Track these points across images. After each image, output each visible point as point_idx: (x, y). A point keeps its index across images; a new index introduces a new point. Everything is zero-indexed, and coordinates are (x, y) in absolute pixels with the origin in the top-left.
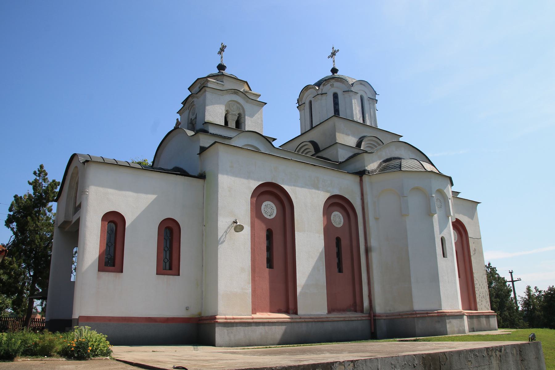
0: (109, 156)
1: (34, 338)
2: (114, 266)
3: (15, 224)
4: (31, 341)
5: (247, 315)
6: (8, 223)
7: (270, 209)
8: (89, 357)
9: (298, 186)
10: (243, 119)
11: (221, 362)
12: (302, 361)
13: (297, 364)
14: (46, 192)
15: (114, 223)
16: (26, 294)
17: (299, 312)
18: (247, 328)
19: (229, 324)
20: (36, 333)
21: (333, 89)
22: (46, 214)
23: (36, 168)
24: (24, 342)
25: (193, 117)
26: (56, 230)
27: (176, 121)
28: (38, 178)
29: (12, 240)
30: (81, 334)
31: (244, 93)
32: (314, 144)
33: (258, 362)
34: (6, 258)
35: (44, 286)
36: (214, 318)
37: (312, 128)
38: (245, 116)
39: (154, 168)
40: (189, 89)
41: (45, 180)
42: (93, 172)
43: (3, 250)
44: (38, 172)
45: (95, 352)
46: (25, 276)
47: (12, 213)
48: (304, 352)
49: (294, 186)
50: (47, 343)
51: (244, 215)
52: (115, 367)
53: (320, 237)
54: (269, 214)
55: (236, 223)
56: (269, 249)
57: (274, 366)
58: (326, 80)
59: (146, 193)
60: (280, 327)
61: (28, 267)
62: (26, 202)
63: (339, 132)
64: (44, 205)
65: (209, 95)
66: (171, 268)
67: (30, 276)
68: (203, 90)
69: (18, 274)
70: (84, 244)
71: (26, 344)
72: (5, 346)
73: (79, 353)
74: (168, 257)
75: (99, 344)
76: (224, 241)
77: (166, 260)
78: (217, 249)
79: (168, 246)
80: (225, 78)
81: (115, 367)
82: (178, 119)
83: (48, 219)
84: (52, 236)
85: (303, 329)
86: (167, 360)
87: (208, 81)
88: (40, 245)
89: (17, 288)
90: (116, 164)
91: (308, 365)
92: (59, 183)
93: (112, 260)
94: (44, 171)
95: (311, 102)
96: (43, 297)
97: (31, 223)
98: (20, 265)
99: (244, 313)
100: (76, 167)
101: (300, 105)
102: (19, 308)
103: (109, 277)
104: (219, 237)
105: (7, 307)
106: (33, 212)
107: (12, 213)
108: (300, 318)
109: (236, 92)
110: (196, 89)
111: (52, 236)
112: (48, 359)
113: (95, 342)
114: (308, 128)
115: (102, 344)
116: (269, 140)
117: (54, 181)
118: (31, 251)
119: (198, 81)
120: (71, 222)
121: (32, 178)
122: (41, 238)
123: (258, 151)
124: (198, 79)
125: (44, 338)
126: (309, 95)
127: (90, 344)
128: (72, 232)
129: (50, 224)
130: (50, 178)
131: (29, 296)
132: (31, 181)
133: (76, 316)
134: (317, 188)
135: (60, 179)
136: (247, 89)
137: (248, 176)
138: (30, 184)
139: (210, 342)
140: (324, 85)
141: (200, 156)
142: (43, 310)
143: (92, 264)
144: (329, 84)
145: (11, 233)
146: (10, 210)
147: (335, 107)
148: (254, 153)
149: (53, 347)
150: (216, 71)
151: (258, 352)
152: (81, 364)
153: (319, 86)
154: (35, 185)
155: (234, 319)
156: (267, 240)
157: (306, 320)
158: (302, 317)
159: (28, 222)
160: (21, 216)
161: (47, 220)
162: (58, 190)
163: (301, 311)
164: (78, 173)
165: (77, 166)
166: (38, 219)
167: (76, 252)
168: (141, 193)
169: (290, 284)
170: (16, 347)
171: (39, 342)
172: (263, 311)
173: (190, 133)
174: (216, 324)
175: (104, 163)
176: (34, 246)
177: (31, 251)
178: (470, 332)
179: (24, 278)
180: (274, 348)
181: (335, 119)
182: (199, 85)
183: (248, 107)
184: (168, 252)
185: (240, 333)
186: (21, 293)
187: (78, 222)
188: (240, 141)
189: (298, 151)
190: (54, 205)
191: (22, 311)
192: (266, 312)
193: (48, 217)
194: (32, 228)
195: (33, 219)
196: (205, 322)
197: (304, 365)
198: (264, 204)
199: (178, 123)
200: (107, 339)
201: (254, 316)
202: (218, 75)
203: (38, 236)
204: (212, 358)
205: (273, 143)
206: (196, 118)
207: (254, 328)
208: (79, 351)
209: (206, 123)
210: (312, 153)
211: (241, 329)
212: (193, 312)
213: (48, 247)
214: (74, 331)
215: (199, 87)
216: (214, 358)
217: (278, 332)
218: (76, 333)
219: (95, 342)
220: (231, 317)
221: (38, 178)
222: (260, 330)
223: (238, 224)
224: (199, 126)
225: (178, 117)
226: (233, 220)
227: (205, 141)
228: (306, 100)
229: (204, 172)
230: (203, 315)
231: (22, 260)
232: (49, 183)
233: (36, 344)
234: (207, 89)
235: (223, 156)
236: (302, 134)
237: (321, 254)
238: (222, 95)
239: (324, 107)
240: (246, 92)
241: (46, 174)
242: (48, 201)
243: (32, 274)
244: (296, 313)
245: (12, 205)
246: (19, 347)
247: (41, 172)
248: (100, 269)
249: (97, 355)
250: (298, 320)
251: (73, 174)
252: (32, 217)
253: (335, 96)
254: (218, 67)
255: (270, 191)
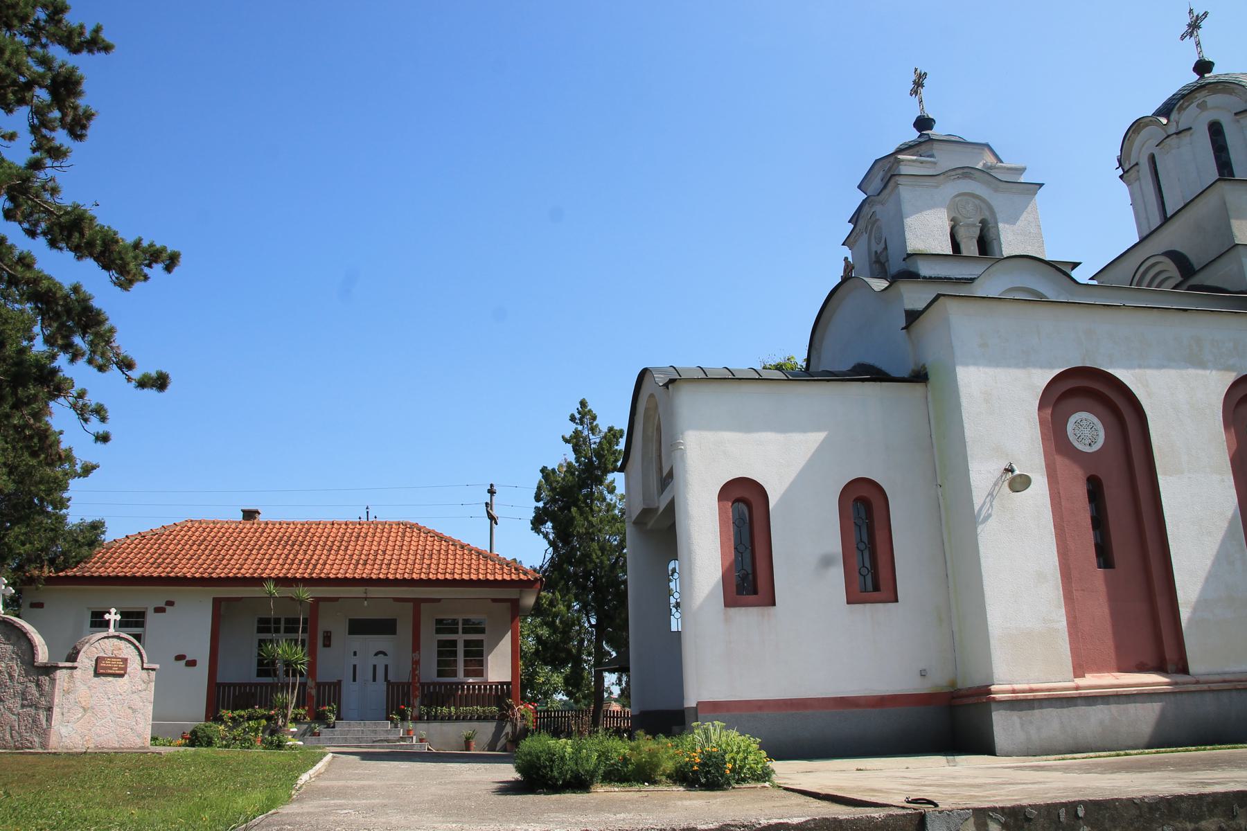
0: (715, 363)
1: (620, 748)
2: (755, 592)
3: (549, 524)
4: (615, 754)
5: (1062, 680)
6: (537, 523)
7: (1088, 430)
8: (729, 784)
9: (1149, 367)
10: (992, 230)
11: (1012, 788)
12: (1208, 784)
13: (1195, 791)
14: (599, 453)
15: (745, 501)
16: (588, 660)
17: (1194, 667)
18: (1065, 710)
19: (1022, 704)
20: (621, 738)
21: (1205, 113)
22: (604, 499)
23: (574, 408)
24: (604, 755)
25: (880, 248)
26: (629, 530)
27: (843, 264)
28: (580, 428)
29: (548, 556)
30: (708, 739)
31: (986, 171)
32: (1177, 258)
33: (1098, 788)
34: (543, 593)
35: (621, 644)
36: (985, 691)
37: (1166, 220)
38: (996, 223)
39: (810, 373)
40: (859, 187)
41: (593, 430)
42: (687, 403)
43: (536, 579)
44: (578, 416)
45: (739, 773)
46: (581, 627)
47: (541, 504)
48: (1213, 764)
49: (1140, 367)
50: (644, 757)
51: (1029, 451)
52: (785, 803)
53: (1223, 481)
54: (1087, 442)
55: (1012, 471)
56: (1099, 522)
57: (1139, 795)
58: (1183, 96)
59: (804, 430)
60: (1148, 705)
61: (585, 608)
62: (563, 479)
63: (1238, 218)
64: (600, 481)
65: (906, 193)
66: (876, 588)
67: (591, 626)
68: (891, 184)
69: (568, 624)
70: (690, 552)
71: (607, 759)
72: (571, 764)
73: (707, 776)
74: (867, 564)
75: (746, 758)
76: (990, 515)
77: (864, 571)
78: (977, 535)
79: (865, 538)
80: (936, 145)
81: (785, 803)
82: (846, 259)
83: (610, 507)
84: (623, 541)
85: (1209, 707)
86: (891, 786)
87: (899, 162)
88: (602, 562)
89: (569, 651)
90: (731, 378)
91: (1226, 794)
92: (622, 431)
93: (749, 581)
94: (590, 411)
95: (1152, 159)
96: (621, 667)
97: (579, 520)
98: (569, 607)
99: (1055, 674)
100: (652, 396)
101: (1127, 170)
102: (579, 690)
103: (747, 617)
104: (977, 508)
105: (555, 690)
106: (581, 497)
107: (541, 504)
108: (1197, 682)
109: (966, 172)
110: (876, 184)
111: (623, 541)
112: (652, 788)
113: (738, 753)
114: (1156, 220)
115: (751, 757)
116: (1062, 270)
117: (611, 429)
118: (587, 575)
119: (877, 167)
120: (657, 509)
121: (570, 429)
122: (602, 549)
123: (1039, 300)
124: (877, 161)
125: (638, 747)
126: (1148, 138)
127: (727, 757)
128: (661, 529)
129: (614, 518)
130: (603, 425)
131: (595, 665)
132: (567, 436)
133: (691, 702)
134: (1201, 365)
135: (622, 424)
136: (990, 160)
137: (1026, 360)
138: (567, 441)
139: (983, 745)
140: (1181, 109)
141: (908, 332)
142: (625, 694)
143: (712, 593)
144: (1194, 105)
145: (545, 544)
146: (538, 499)
147: (1217, 158)
148: (1029, 308)
149: (657, 766)
150: (913, 135)
151: (1097, 765)
152: (715, 798)
153: (1167, 115)
154: (576, 441)
155: (1032, 691)
156: (1090, 501)
157: (1213, 686)
158: (1202, 679)
159: (573, 518)
160: (560, 509)
161: (608, 511)
162: (621, 446)
163: (1198, 664)
164: (656, 407)
165: (654, 394)
166: (591, 509)
167: (674, 571)
168: (792, 431)
169: (1161, 602)
170: (590, 766)
171: (631, 755)
172: (1100, 668)
173: (879, 284)
174: (993, 706)
175: (706, 379)
176: (590, 566)
177: (586, 577)
178: (258, 675)
179: (579, 633)
180: (1136, 756)
181: (1225, 187)
182: (881, 173)
183: (999, 201)
184: (866, 554)
185: (1052, 723)
186: (577, 661)
187: (671, 508)
188: (993, 284)
189: (1149, 285)
190: (618, 479)
191: (584, 697)
192: (1109, 670)
193: (609, 504)
194: (582, 530)
195: (582, 513)
196: (965, 701)
197: (1214, 795)
198: (1072, 419)
199: (849, 267)
200: (762, 747)
201: (1080, 682)
202: (920, 144)
203: (595, 545)
204: (991, 781)
205: (1074, 274)
206: (886, 248)
207: (1083, 709)
208: (709, 772)
209: (909, 255)
210: (1173, 282)
211: (1052, 712)
212: (936, 681)
213: (619, 565)
214: (692, 732)
215: (884, 178)
216: (996, 781)
217: (1146, 717)
218: (698, 736)
219: (738, 753)
220: (1025, 686)
221: (580, 428)
222: (1097, 716)
223: (1017, 472)
224: (895, 266)
225: (846, 252)
226: (1005, 465)
227: (914, 296)
228: (1141, 155)
229: (924, 367)
230: (959, 686)
231: (571, 596)
232: (602, 434)
233: (625, 761)
234: (901, 180)
235: (961, 324)
236: (1142, 240)
237: (1232, 523)
238: (936, 187)
239: (1190, 162)
240: (991, 168)
241: (594, 418)
242: (606, 471)
243: (593, 621)
244: (1184, 670)
245: (539, 488)
246: (597, 766)
247: (584, 414)
248: (729, 603)
249: (744, 780)
250: (1192, 687)
251: (647, 410)
252: (579, 508)
253: (1216, 130)
254: (915, 125)
255: (1082, 389)
